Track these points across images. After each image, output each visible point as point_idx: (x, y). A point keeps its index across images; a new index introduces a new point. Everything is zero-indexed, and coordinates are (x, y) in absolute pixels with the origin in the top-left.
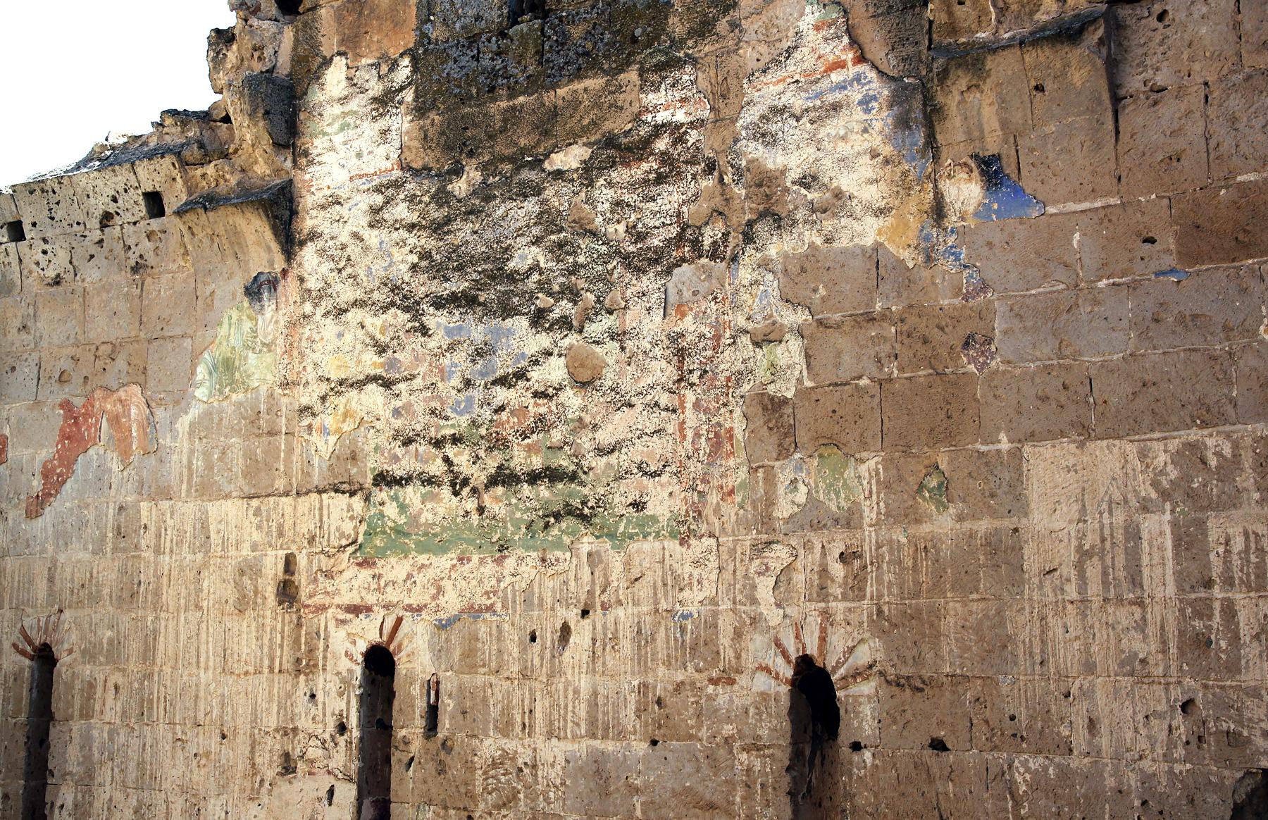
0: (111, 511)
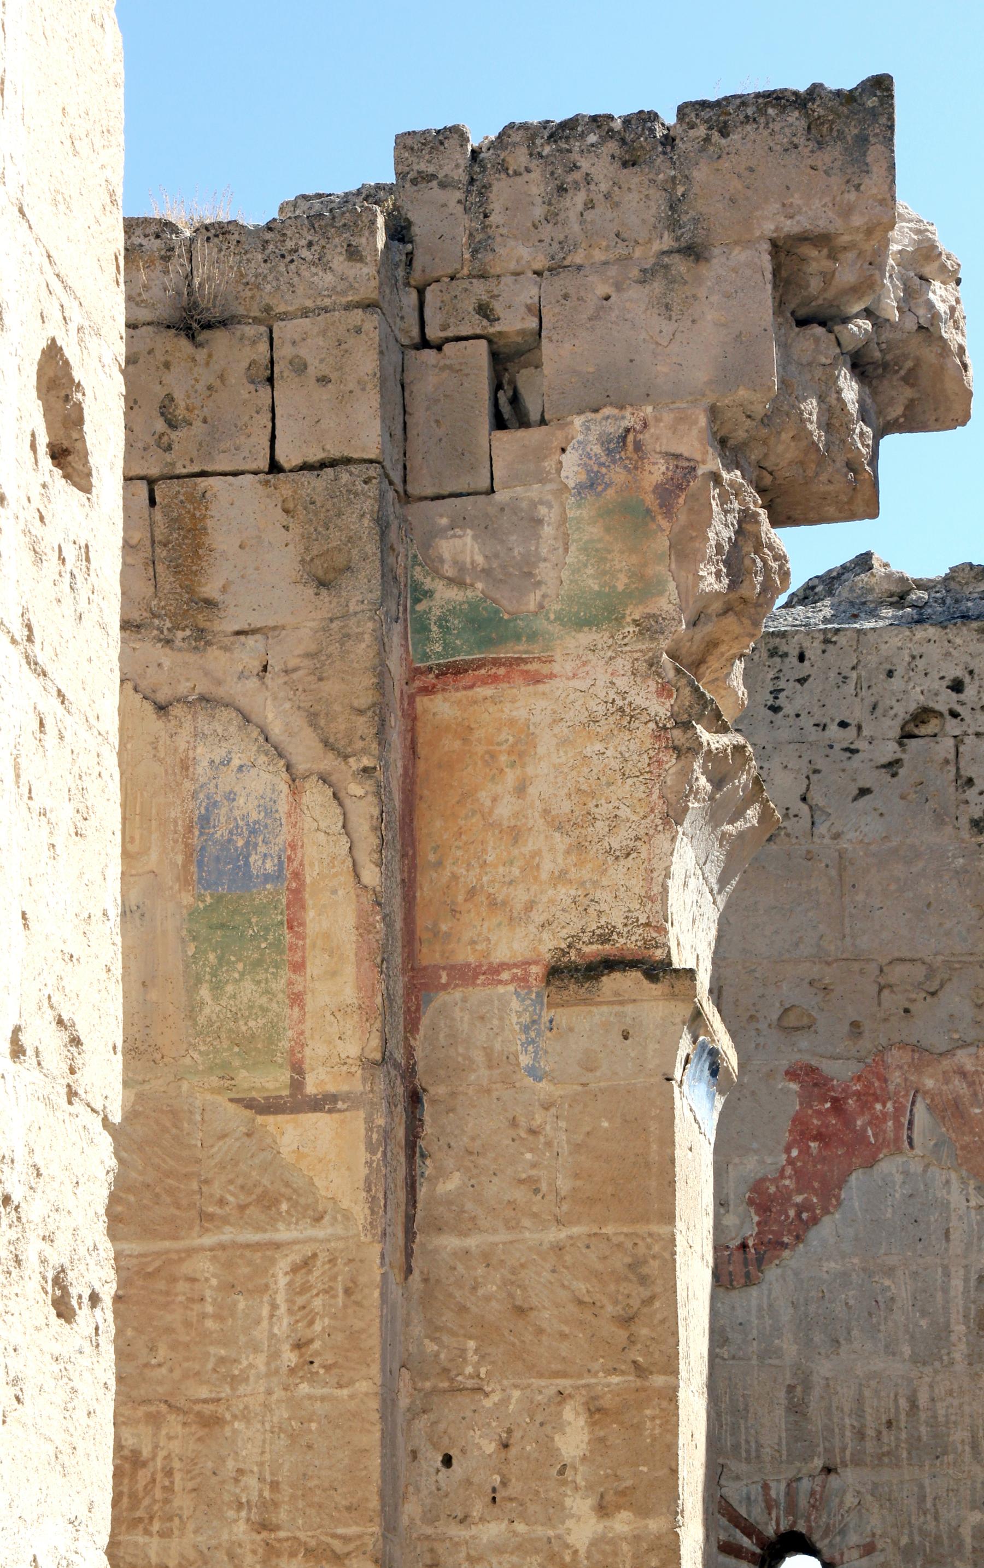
0: (957, 1283)
